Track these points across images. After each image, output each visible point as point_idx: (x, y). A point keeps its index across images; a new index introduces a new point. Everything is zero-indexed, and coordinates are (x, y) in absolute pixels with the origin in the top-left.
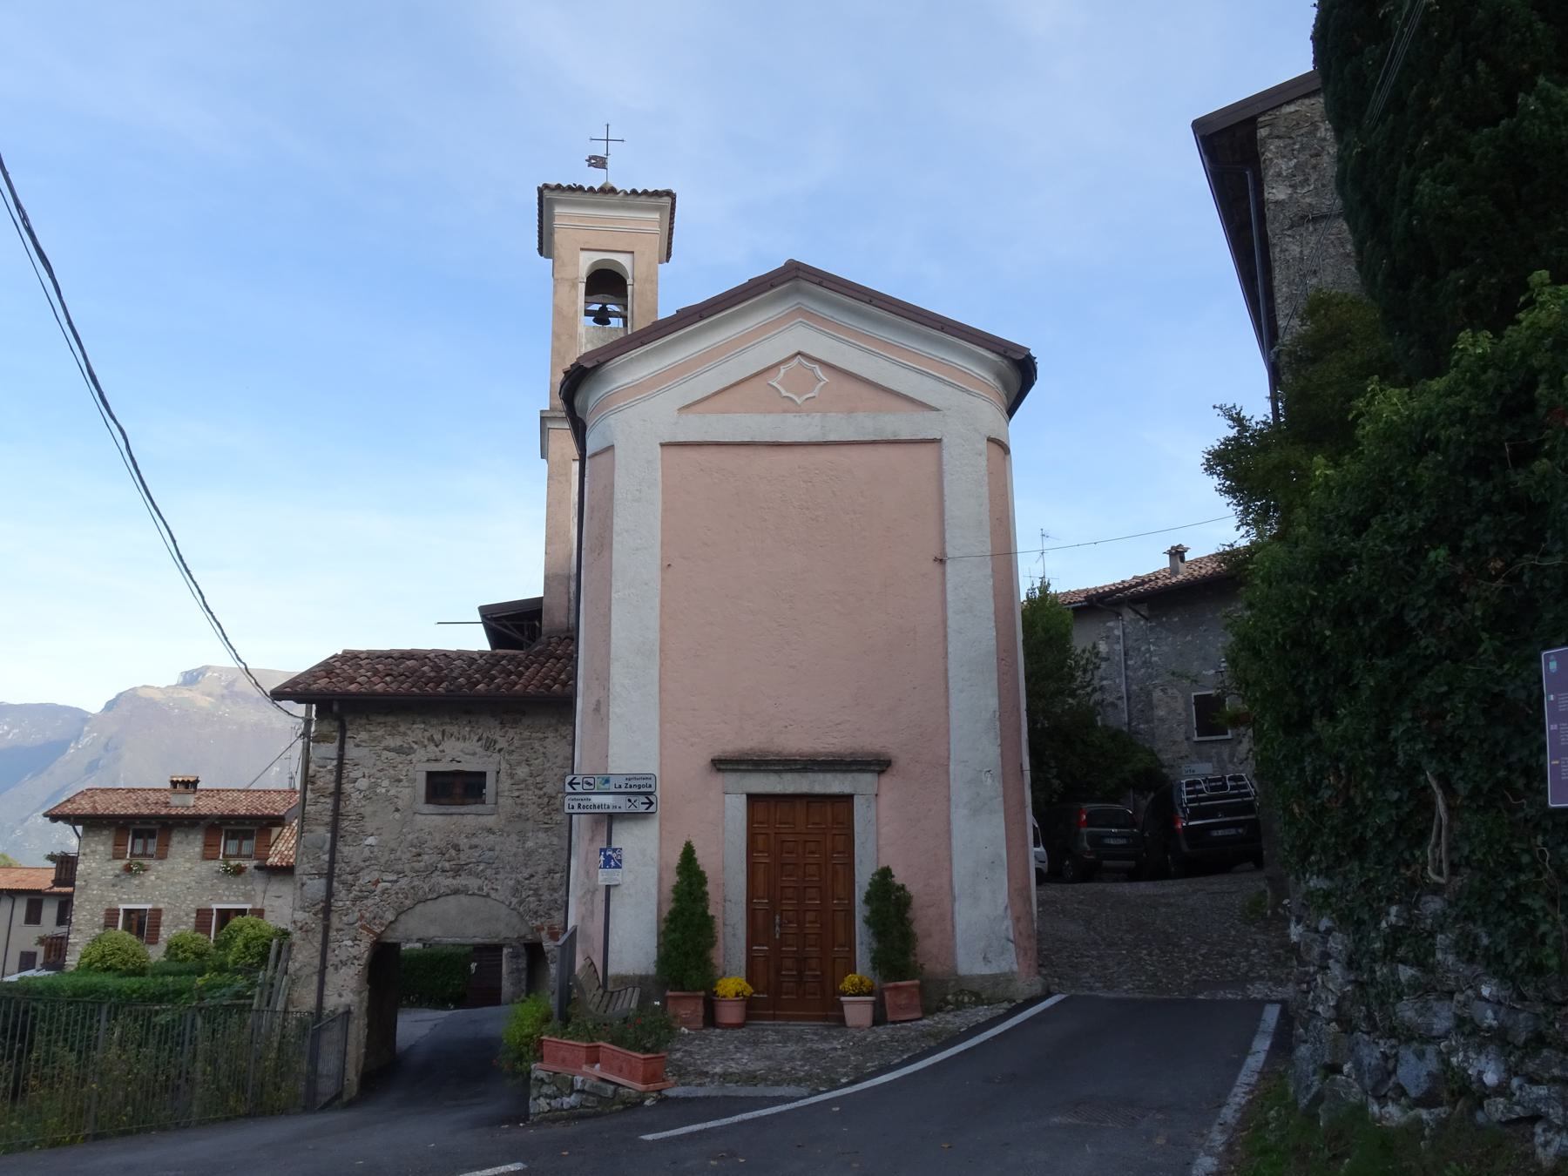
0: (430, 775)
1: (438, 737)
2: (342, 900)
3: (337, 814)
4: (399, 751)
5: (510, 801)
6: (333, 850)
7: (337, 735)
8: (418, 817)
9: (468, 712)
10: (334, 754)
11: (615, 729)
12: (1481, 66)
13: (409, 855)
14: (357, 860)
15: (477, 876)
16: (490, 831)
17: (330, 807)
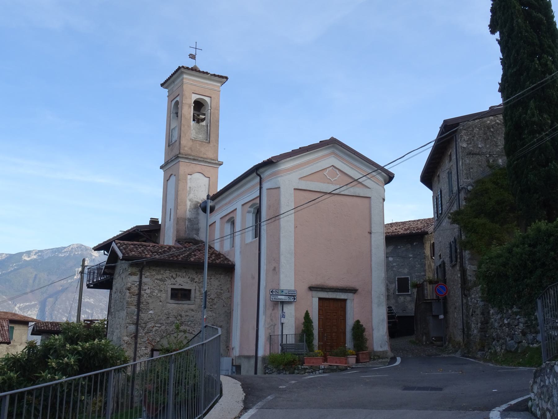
0: (172, 289)
1: (174, 276)
2: (141, 333)
3: (139, 303)
4: (161, 280)
5: (199, 300)
6: (138, 315)
7: (139, 273)
8: (168, 304)
9: (185, 268)
10: (138, 280)
11: (282, 276)
12: (542, 155)
13: (165, 318)
14: (146, 319)
15: (188, 326)
16: (192, 310)
17: (136, 299)
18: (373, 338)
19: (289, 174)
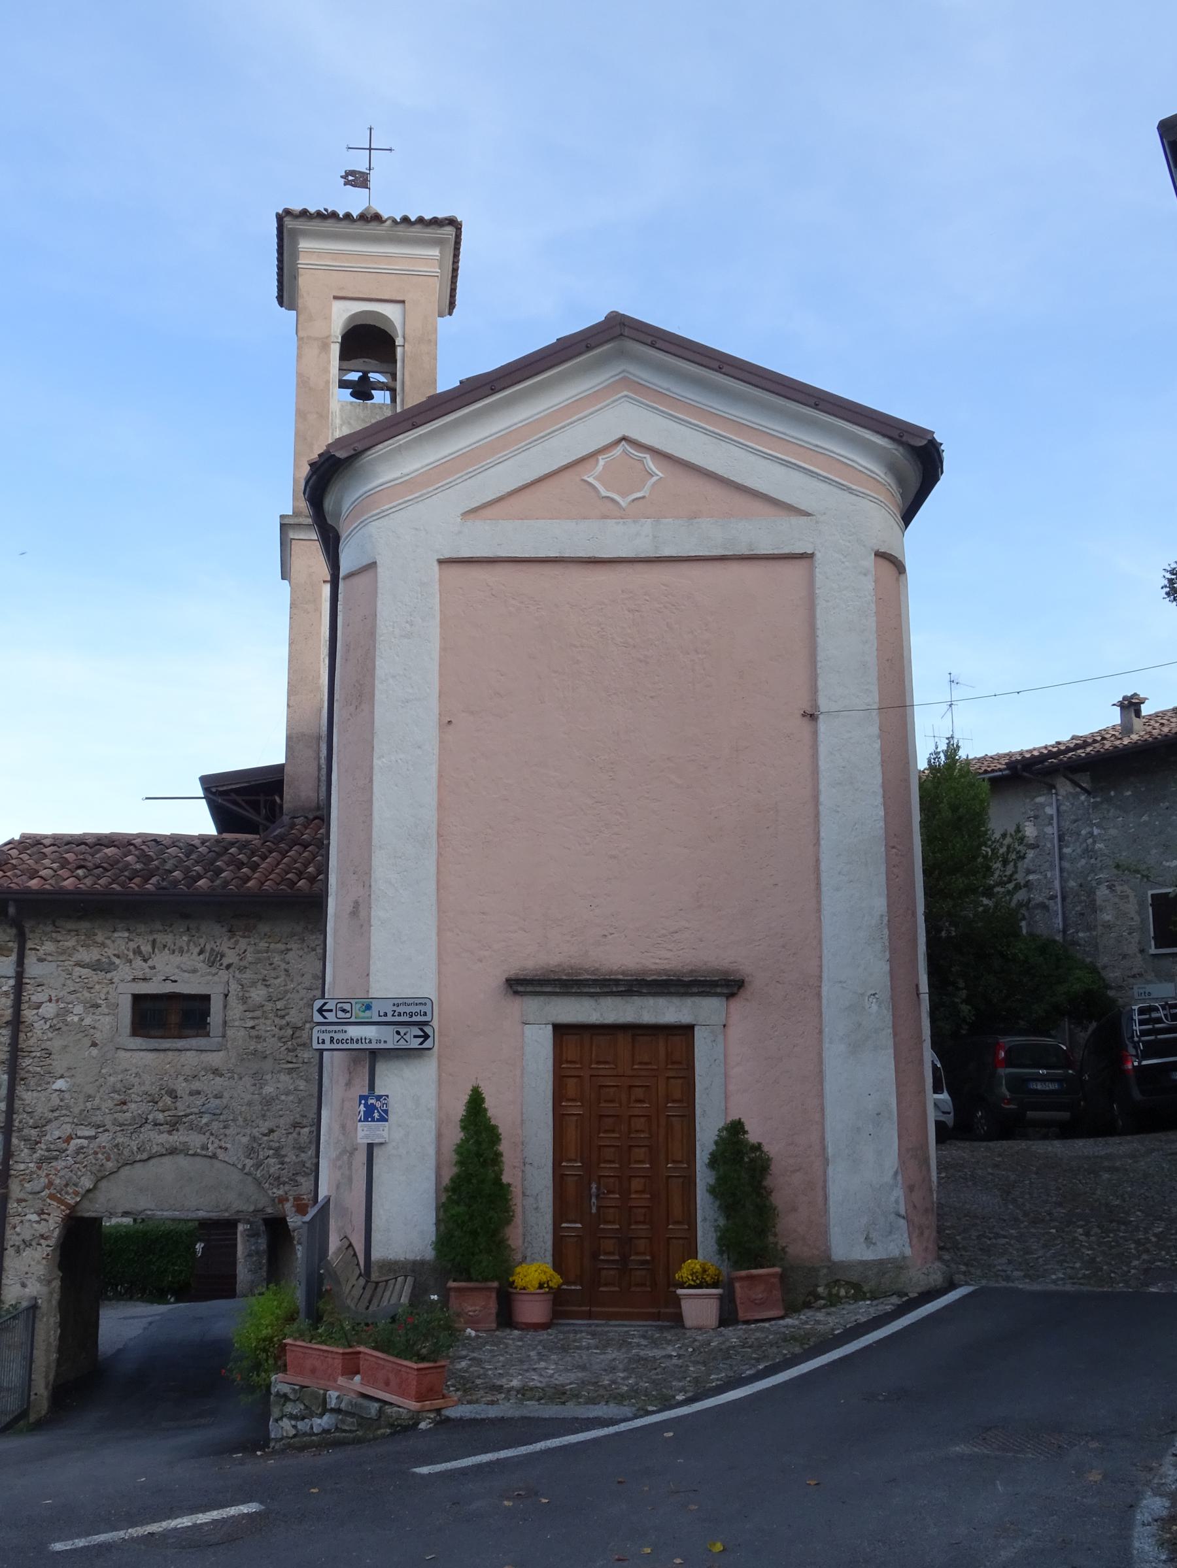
0: (137, 998)
1: (146, 949)
4: (96, 967)
5: (242, 1032)
7: (14, 945)
8: (121, 1054)
9: (185, 916)
13: (110, 1104)
15: (201, 1130)
16: (216, 1072)
18: (826, 1198)
19: (416, 500)
